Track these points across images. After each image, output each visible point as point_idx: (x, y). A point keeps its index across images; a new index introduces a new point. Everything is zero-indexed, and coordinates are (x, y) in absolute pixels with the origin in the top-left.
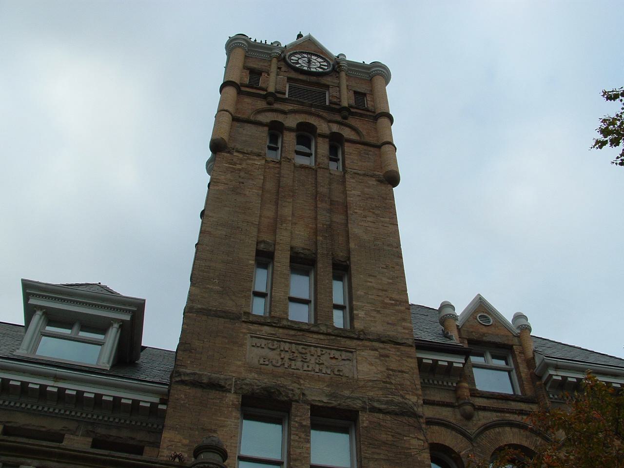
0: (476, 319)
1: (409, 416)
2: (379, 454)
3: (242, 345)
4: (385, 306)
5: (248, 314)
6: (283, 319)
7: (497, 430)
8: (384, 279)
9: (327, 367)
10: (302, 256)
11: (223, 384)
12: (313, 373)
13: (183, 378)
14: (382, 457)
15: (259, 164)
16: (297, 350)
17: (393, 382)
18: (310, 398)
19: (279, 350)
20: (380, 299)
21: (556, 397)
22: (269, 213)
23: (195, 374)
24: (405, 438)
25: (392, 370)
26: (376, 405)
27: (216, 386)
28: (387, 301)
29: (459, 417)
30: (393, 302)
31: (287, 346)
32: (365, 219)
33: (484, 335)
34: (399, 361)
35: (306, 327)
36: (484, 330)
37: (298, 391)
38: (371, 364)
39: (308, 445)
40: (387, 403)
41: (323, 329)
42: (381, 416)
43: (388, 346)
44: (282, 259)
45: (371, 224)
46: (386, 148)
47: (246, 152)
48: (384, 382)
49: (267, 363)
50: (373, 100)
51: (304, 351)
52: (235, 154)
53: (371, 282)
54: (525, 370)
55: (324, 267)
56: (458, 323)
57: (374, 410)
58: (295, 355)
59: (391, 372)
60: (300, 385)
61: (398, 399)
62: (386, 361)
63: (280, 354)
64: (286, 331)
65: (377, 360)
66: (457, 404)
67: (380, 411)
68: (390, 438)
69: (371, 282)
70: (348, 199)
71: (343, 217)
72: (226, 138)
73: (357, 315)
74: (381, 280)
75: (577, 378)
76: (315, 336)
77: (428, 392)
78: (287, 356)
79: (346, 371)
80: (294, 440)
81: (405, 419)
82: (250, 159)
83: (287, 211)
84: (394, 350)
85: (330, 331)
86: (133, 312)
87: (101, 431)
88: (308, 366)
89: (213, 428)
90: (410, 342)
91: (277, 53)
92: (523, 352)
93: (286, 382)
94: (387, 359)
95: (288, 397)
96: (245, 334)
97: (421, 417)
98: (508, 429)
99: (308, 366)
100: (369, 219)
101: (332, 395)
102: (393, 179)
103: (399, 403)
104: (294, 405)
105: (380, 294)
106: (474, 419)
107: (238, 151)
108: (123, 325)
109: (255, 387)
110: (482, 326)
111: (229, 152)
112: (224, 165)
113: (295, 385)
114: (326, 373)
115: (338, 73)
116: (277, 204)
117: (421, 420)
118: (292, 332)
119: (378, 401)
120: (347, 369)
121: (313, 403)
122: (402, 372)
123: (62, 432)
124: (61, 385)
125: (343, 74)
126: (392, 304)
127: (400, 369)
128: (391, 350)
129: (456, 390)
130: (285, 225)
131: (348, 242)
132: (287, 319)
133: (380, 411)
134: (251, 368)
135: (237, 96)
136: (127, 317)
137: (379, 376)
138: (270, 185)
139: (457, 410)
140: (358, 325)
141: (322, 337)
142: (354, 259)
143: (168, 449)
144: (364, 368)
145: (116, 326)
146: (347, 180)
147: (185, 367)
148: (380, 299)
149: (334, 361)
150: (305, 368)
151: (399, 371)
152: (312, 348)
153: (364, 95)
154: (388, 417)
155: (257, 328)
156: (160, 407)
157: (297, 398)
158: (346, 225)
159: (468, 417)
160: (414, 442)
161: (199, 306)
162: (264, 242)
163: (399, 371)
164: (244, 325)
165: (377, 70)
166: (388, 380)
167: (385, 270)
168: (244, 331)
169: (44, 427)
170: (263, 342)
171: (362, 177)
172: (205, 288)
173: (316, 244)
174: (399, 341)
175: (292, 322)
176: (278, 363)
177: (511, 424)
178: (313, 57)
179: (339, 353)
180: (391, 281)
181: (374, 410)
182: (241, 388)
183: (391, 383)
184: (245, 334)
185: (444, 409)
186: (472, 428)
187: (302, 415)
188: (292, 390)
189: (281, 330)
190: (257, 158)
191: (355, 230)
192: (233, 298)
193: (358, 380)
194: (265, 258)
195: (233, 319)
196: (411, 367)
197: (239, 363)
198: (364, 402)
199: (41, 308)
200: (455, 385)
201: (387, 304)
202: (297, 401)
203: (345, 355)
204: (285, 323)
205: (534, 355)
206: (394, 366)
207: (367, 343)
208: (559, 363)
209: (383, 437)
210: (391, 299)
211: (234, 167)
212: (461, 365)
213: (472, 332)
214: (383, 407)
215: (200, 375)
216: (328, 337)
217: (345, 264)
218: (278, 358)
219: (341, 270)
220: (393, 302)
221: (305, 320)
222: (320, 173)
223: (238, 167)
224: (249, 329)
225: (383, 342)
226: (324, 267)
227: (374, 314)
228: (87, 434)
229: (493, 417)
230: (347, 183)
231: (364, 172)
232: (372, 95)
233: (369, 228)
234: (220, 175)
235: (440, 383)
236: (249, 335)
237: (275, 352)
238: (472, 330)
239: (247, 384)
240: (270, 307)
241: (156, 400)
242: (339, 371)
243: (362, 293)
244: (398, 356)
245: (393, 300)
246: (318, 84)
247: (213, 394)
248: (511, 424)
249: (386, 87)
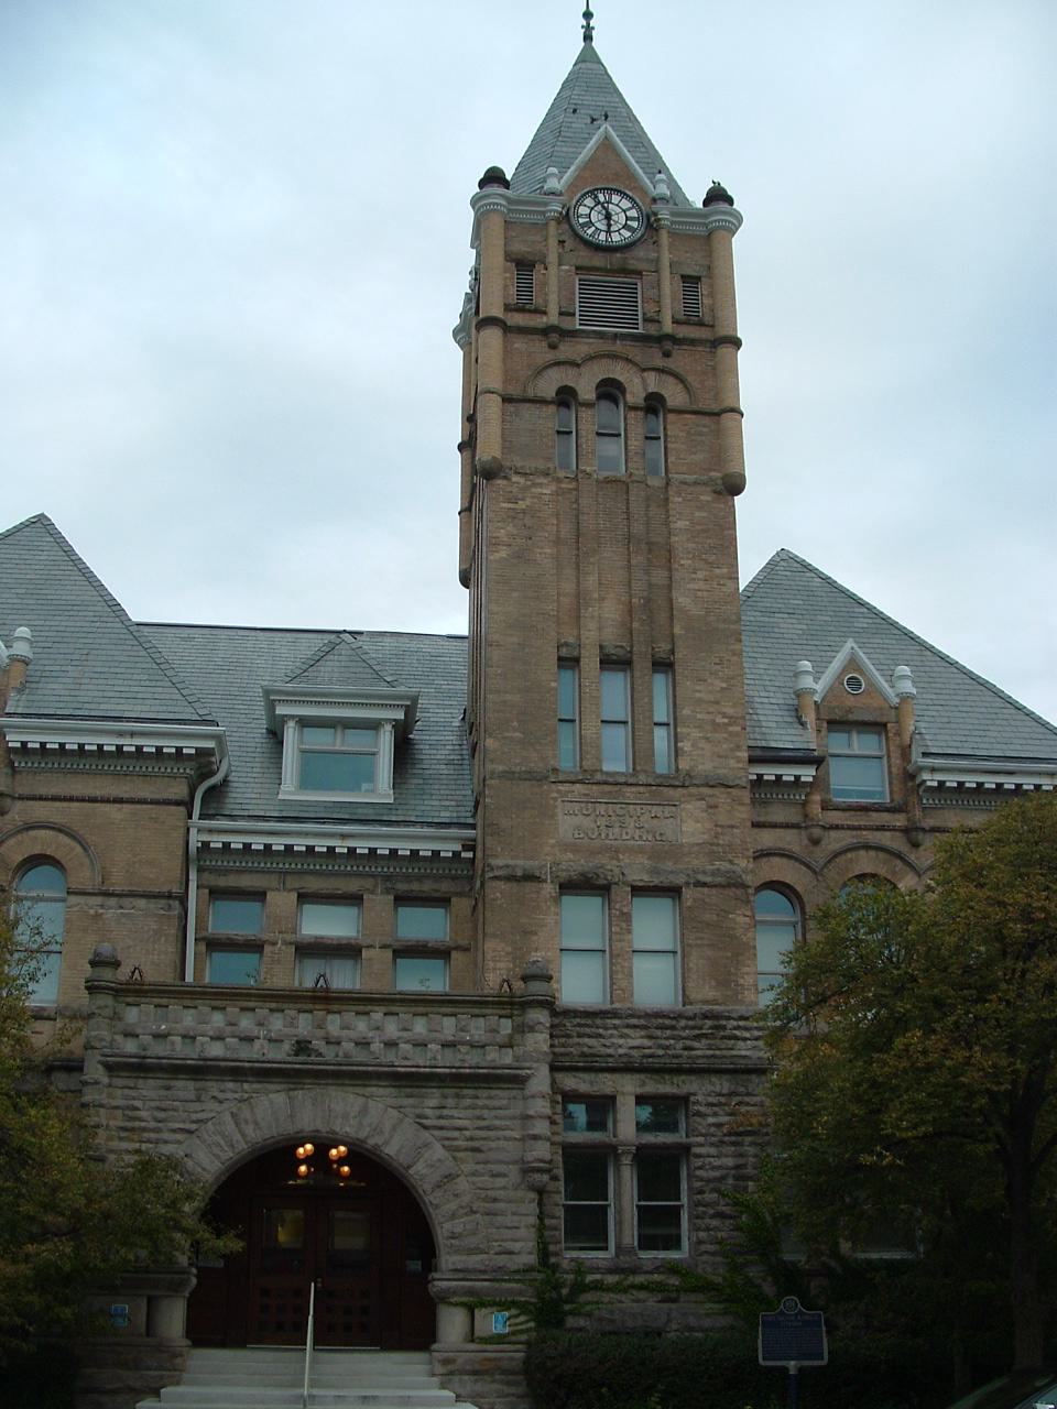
1: (737, 888)
2: (702, 938)
3: (553, 816)
6: (597, 771)
7: (849, 855)
8: (717, 682)
9: (648, 832)
10: (615, 658)
12: (632, 842)
13: (497, 873)
14: (706, 942)
16: (614, 812)
17: (721, 842)
19: (593, 815)
22: (568, 587)
23: (507, 866)
25: (721, 826)
27: (530, 877)
28: (720, 720)
30: (726, 721)
31: (601, 809)
32: (694, 576)
33: (850, 710)
34: (729, 811)
35: (622, 780)
36: (850, 702)
37: (617, 871)
39: (630, 937)
40: (713, 874)
41: (642, 778)
42: (706, 890)
43: (716, 791)
44: (590, 662)
45: (701, 585)
46: (727, 418)
48: (711, 845)
49: (581, 836)
50: (712, 295)
51: (621, 812)
52: (515, 479)
53: (700, 691)
55: (642, 664)
56: (817, 698)
57: (699, 884)
58: (613, 818)
59: (719, 830)
60: (618, 860)
61: (725, 866)
62: (714, 814)
63: (596, 822)
65: (705, 814)
67: (705, 885)
68: (715, 917)
69: (700, 691)
71: (666, 574)
72: (498, 455)
73: (682, 749)
76: (633, 789)
78: (602, 822)
81: (731, 892)
82: (534, 485)
83: (591, 581)
84: (724, 796)
85: (650, 781)
86: (407, 706)
87: (402, 887)
90: (743, 782)
91: (555, 211)
92: (898, 734)
94: (716, 810)
95: (606, 879)
97: (749, 887)
98: (862, 853)
99: (627, 833)
102: (735, 486)
104: (613, 886)
105: (711, 710)
106: (823, 842)
108: (397, 725)
109: (572, 874)
111: (505, 478)
113: (614, 862)
114: (647, 840)
115: (656, 230)
116: (578, 567)
119: (704, 872)
122: (732, 827)
125: (664, 237)
129: (804, 804)
131: (672, 626)
132: (601, 771)
133: (705, 885)
134: (566, 847)
135: (504, 341)
137: (706, 837)
140: (684, 765)
141: (641, 789)
144: (689, 826)
145: (388, 727)
146: (671, 498)
147: (496, 857)
148: (711, 717)
149: (655, 821)
152: (631, 806)
153: (697, 279)
154: (714, 891)
155: (567, 789)
156: (463, 855)
158: (670, 587)
159: (816, 842)
160: (741, 919)
161: (501, 768)
162: (566, 644)
164: (553, 786)
165: (719, 221)
166: (716, 841)
167: (719, 667)
168: (555, 795)
169: (338, 889)
170: (577, 806)
172: (505, 738)
173: (631, 633)
174: (731, 784)
177: (867, 847)
178: (616, 198)
180: (724, 685)
181: (699, 884)
183: (718, 845)
184: (555, 799)
186: (819, 856)
187: (621, 893)
188: (611, 871)
189: (594, 787)
190: (545, 481)
191: (682, 600)
192: (538, 747)
193: (682, 845)
194: (569, 662)
195: (540, 780)
198: (688, 875)
200: (803, 798)
201: (719, 725)
202: (616, 884)
204: (598, 777)
205: (911, 741)
206: (723, 819)
209: (707, 917)
210: (724, 715)
212: (811, 779)
214: (708, 879)
215: (514, 867)
216: (649, 788)
218: (593, 825)
219: (664, 665)
220: (726, 721)
222: (634, 489)
223: (522, 505)
224: (559, 792)
225: (712, 786)
226: (642, 664)
227: (702, 744)
228: (387, 891)
229: (844, 839)
231: (693, 477)
232: (710, 278)
233: (699, 593)
239: (563, 870)
240: (581, 754)
242: (661, 834)
243: (689, 712)
245: (727, 717)
246: (625, 271)
247: (529, 886)
248: (867, 847)
249: (733, 239)
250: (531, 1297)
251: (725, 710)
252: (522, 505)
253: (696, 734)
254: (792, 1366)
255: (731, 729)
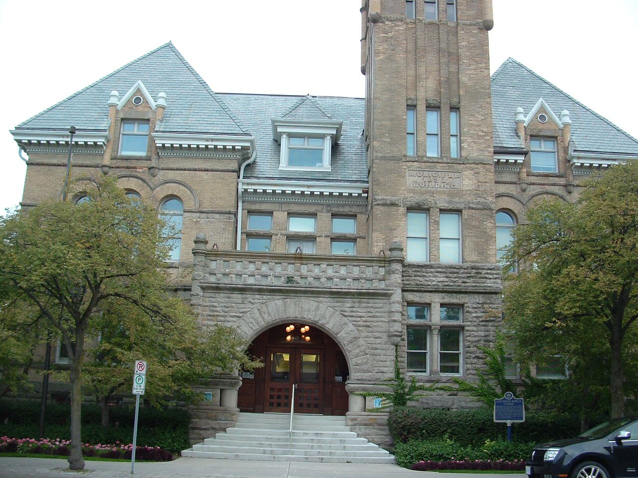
0: (537, 118)
4: (479, 137)
5: (405, 156)
6: (424, 156)
8: (480, 116)
11: (397, 203)
12: (440, 189)
13: (379, 203)
15: (402, 29)
17: (481, 189)
18: (439, 205)
20: (477, 132)
21: (577, 173)
22: (412, 72)
24: (485, 223)
25: (480, 182)
26: (471, 205)
28: (480, 134)
29: (519, 190)
30: (483, 134)
31: (426, 174)
32: (469, 67)
37: (433, 202)
38: (470, 180)
41: (445, 160)
42: (473, 211)
43: (479, 166)
44: (421, 107)
45: (473, 72)
47: (393, 19)
48: (476, 190)
53: (471, 120)
54: (562, 154)
55: (445, 108)
57: (470, 208)
58: (431, 178)
59: (480, 184)
61: (482, 200)
64: (426, 164)
66: (518, 183)
67: (473, 209)
68: (477, 224)
69: (471, 120)
70: (460, 50)
74: (478, 117)
75: (590, 164)
76: (441, 165)
77: (503, 175)
78: (426, 180)
79: (457, 186)
80: (432, 230)
81: (485, 212)
82: (396, 26)
83: (422, 70)
85: (449, 161)
87: (335, 210)
88: (438, 185)
89: (395, 228)
93: (427, 197)
96: (405, 169)
99: (438, 185)
100: (472, 67)
101: (450, 202)
102: (488, 26)
103: (483, 203)
107: (388, 20)
110: (540, 124)
112: (381, 35)
117: (493, 211)
118: (429, 164)
120: (457, 183)
121: (441, 208)
123: (316, 212)
124: (312, 190)
126: (483, 136)
127: (484, 180)
128: (480, 168)
130: (421, 83)
132: (426, 156)
133: (473, 209)
136: (334, 132)
138: (410, 47)
139: (518, 186)
140: (464, 154)
141: (445, 165)
142: (462, 104)
143: (376, 242)
145: (329, 138)
148: (477, 132)
149: (451, 179)
150: (436, 187)
151: (485, 182)
154: (477, 211)
155: (411, 164)
156: (363, 195)
157: (432, 206)
158: (458, 73)
159: (524, 190)
160: (489, 224)
161: (380, 155)
163: (485, 182)
164: (404, 163)
168: (405, 167)
171: (468, 27)
175: (429, 157)
176: (422, 185)
179: (453, 174)
180: (483, 118)
181: (470, 208)
182: (406, 204)
183: (479, 190)
184: (405, 169)
185: (511, 185)
186: (525, 197)
187: (435, 212)
191: (464, 79)
193: (463, 190)
194: (412, 107)
196: (491, 179)
197: (403, 188)
199: (285, 133)
200: (518, 170)
203: (457, 175)
204: (425, 159)
207: (468, 166)
208: (580, 156)
209: (474, 223)
211: (387, 35)
212: (522, 162)
213: (533, 129)
214: (475, 206)
216: (448, 164)
217: (457, 106)
219: (455, 109)
220: (483, 134)
221: (436, 156)
222: (441, 27)
223: (390, 35)
224: (407, 166)
226: (445, 108)
228: (328, 211)
229: (538, 189)
230: (459, 35)
233: (472, 76)
234: (379, 45)
235: (510, 170)
236: (407, 169)
237: (421, 178)
238: (533, 127)
241: (360, 192)
243: (467, 130)
244: (484, 172)
245: (484, 132)
247: (393, 208)
250: (391, 392)
251: (482, 129)
252: (390, 35)
253: (470, 140)
254: (509, 423)
255: (486, 138)
